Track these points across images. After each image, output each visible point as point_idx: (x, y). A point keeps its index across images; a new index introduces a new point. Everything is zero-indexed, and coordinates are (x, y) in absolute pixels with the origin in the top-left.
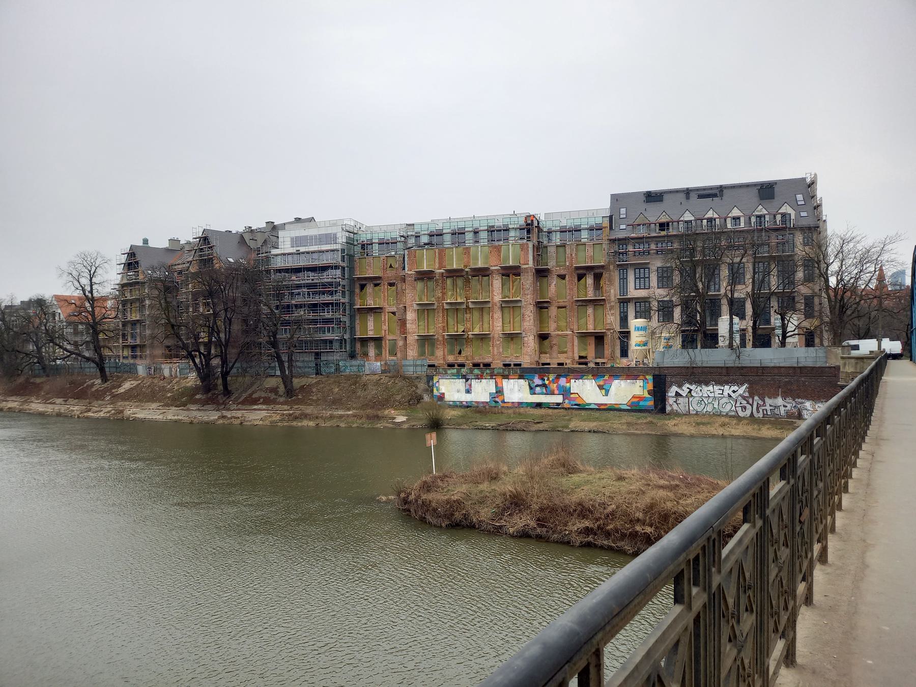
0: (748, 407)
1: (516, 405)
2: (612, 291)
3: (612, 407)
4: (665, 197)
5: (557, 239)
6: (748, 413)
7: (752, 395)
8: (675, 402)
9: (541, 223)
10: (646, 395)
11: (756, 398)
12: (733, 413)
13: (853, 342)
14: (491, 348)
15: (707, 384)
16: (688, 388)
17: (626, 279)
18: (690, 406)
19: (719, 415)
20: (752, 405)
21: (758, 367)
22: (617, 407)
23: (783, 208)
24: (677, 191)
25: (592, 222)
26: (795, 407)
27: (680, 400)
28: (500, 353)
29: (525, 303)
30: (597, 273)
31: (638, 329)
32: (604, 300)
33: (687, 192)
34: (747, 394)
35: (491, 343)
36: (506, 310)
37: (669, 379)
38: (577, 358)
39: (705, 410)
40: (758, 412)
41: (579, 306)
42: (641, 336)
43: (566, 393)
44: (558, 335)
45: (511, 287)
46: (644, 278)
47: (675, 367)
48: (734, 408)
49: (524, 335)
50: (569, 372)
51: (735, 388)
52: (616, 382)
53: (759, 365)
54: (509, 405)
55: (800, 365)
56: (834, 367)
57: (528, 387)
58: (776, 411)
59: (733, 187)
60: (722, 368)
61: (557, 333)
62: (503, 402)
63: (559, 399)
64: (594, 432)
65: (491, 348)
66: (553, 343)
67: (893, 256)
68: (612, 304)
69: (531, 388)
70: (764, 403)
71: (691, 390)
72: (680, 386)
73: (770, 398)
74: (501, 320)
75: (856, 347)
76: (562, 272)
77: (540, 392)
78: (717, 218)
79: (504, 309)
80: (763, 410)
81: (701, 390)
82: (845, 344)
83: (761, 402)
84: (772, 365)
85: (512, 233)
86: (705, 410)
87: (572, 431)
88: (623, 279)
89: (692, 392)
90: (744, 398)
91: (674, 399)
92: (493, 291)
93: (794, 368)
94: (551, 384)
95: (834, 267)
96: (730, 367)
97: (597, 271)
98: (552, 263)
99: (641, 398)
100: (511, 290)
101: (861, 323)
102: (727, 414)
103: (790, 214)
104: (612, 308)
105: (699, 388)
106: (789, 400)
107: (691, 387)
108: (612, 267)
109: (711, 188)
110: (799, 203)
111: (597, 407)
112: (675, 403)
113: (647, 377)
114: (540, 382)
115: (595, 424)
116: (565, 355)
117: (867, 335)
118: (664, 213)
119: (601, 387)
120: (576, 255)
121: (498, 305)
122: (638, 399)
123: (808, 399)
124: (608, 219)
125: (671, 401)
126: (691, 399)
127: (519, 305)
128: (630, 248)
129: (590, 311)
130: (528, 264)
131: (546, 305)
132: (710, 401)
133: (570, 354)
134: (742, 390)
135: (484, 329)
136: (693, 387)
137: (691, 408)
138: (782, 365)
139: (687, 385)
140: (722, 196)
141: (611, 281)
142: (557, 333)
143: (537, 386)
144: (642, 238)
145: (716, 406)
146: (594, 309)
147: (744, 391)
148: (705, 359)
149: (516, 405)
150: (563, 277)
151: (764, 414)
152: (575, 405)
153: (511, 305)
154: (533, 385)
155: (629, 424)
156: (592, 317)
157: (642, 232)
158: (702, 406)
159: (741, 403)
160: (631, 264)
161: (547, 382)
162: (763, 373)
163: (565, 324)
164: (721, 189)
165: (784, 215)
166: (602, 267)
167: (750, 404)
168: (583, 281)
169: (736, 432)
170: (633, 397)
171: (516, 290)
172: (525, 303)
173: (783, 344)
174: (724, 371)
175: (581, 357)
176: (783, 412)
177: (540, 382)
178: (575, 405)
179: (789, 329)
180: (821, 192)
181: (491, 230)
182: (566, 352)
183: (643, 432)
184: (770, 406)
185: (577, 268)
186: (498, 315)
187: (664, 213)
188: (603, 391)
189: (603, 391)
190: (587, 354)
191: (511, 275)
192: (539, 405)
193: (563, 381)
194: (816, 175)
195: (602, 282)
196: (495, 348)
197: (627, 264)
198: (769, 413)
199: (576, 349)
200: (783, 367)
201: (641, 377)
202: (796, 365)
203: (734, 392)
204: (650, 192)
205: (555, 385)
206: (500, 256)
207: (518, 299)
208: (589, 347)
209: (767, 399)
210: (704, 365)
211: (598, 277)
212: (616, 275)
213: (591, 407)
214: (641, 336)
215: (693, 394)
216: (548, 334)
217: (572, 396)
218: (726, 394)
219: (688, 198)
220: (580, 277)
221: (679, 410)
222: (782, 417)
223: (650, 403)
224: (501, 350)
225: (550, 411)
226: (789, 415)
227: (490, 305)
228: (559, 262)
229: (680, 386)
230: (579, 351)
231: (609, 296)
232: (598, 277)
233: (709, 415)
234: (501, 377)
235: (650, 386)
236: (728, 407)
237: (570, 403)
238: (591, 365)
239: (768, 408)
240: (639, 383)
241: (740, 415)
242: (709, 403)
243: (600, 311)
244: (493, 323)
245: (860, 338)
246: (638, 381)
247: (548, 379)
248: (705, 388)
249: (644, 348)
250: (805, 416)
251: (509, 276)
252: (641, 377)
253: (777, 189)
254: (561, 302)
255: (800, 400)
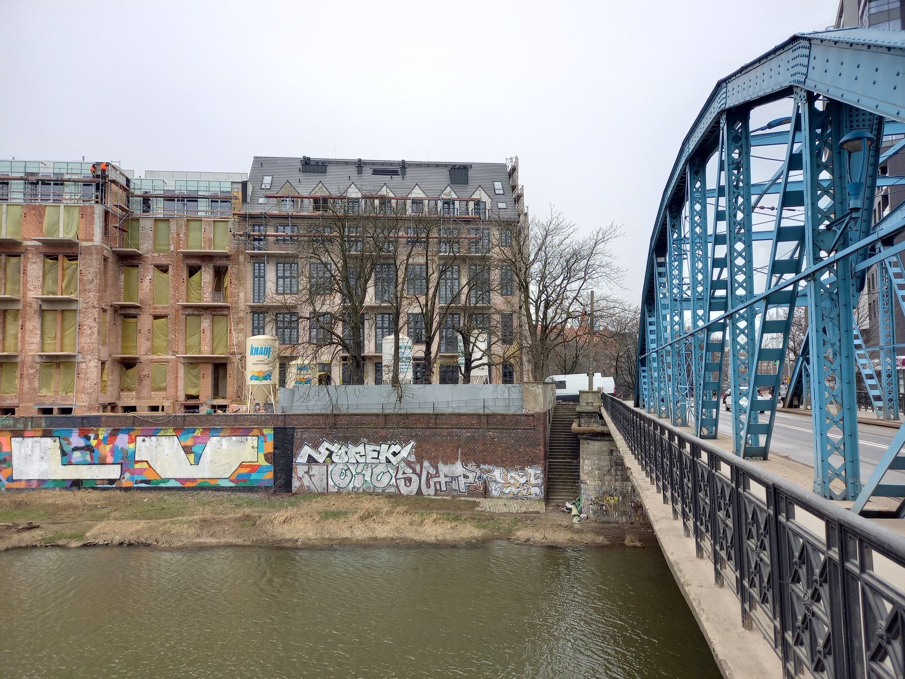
0: (415, 478)
1: (34, 485)
2: (242, 295)
3: (207, 485)
4: (330, 169)
5: (159, 209)
6: (414, 488)
7: (420, 460)
8: (307, 473)
9: (132, 185)
10: (263, 462)
11: (426, 464)
12: (393, 490)
13: (559, 378)
14: (17, 381)
15: (356, 443)
16: (327, 449)
17: (264, 277)
18: (329, 477)
19: (370, 494)
20: (420, 476)
21: (429, 415)
22: (212, 483)
23: (478, 192)
24: (346, 163)
25: (215, 189)
26: (480, 477)
27: (315, 469)
28: (34, 389)
29: (85, 305)
30: (219, 267)
31: (255, 351)
32: (228, 308)
33: (360, 165)
34: (413, 458)
35: (18, 374)
36: (49, 317)
37: (298, 435)
38: (182, 398)
39: (351, 486)
40: (428, 486)
41: (189, 315)
42: (261, 362)
43: (126, 461)
44: (153, 361)
45: (60, 277)
46: (291, 277)
47: (310, 415)
48: (393, 480)
49: (79, 358)
50: (134, 424)
51: (396, 448)
52: (214, 440)
53: (431, 411)
54: (22, 485)
55: (487, 412)
56: (533, 415)
57: (59, 452)
58: (454, 486)
59: (419, 165)
60: (377, 415)
61: (150, 357)
62: (10, 479)
63: (113, 472)
64: (130, 545)
65: (17, 381)
66: (144, 373)
67: (608, 259)
68: (241, 314)
69: (64, 453)
70: (437, 472)
71: (331, 453)
72: (316, 447)
73: (445, 463)
74: (39, 332)
75: (562, 385)
76: (163, 261)
77: (81, 460)
78: (393, 198)
79: (46, 314)
80: (435, 483)
81: (346, 453)
82: (548, 380)
83: (432, 471)
84: (450, 411)
85: (69, 189)
86: (351, 486)
87: (85, 546)
88: (259, 277)
89: (334, 456)
90: (409, 464)
91: (306, 468)
92: (25, 283)
93: (480, 415)
94: (102, 446)
95: (536, 268)
96: (389, 414)
97: (220, 263)
98: (146, 245)
99: (254, 468)
100: (60, 282)
101: (570, 353)
102: (383, 491)
103: (485, 202)
104: (240, 321)
105: (344, 449)
106: (472, 466)
107: (333, 448)
108: (241, 258)
109: (391, 164)
110: (497, 192)
111: (178, 484)
112: (306, 475)
113: (265, 432)
114: (81, 443)
115: (142, 524)
116: (162, 394)
117: (572, 368)
118: (320, 184)
119: (187, 450)
120: (186, 235)
121: (35, 306)
122: (249, 469)
123: (497, 465)
124: (240, 186)
125: (300, 471)
126: (330, 468)
127: (73, 307)
128: (271, 231)
129: (206, 323)
130: (92, 240)
131: (133, 312)
132: (359, 470)
133: (171, 391)
134: (406, 451)
135: (7, 348)
136: (334, 448)
137: (331, 483)
138: (463, 411)
139: (326, 445)
140: (404, 174)
141: (240, 279)
142: (150, 357)
143: (76, 449)
144: (286, 217)
145: (368, 478)
146: (213, 322)
147: (409, 454)
148: (353, 401)
149: (34, 485)
150: (164, 269)
151: (436, 490)
152: (142, 481)
153: (60, 307)
154: (67, 449)
155: (205, 523)
156: (208, 333)
157: (287, 208)
158: (348, 479)
159: (404, 473)
160: (270, 256)
161: (93, 443)
162: (436, 424)
163: (165, 344)
164: (404, 165)
165: (478, 203)
166: (227, 257)
167: (417, 474)
168: (196, 277)
169: (383, 531)
170: (241, 466)
171: (69, 282)
172: (85, 305)
173: (467, 379)
174: (381, 420)
175: (189, 397)
176: (463, 488)
177: (81, 443)
178: (142, 481)
179: (475, 356)
180: (523, 179)
181: (34, 182)
182: (165, 389)
183: (223, 540)
184: (446, 476)
185: (187, 256)
186: (33, 324)
187: (320, 184)
188: (192, 457)
189: (192, 457)
190: (199, 392)
191: (60, 257)
192: (77, 484)
193: (122, 440)
194: (517, 158)
195: (227, 281)
196: (26, 382)
197: (263, 255)
198: (444, 489)
199: (181, 383)
200: (464, 415)
201: (256, 432)
202: (481, 412)
203: (395, 454)
204: (309, 159)
205: (108, 447)
206: (41, 223)
207: (73, 297)
208: (202, 381)
209: (441, 466)
210: (351, 411)
211: (220, 274)
212: (248, 270)
213: (169, 484)
214: (261, 362)
215: (335, 458)
216: (136, 359)
217: (137, 466)
218: (382, 458)
219: (360, 172)
220: (193, 271)
221: (312, 487)
222: (461, 494)
223: (268, 476)
224: (36, 384)
225: (95, 495)
226: (471, 491)
227: (20, 306)
228: (159, 245)
229: (316, 447)
230: (186, 385)
231: (237, 302)
232: (220, 274)
233: (357, 493)
234: (9, 435)
235: (269, 447)
236: (386, 480)
237: (132, 479)
238: (204, 410)
239: (443, 480)
240: (252, 441)
241: (402, 492)
242: (358, 474)
243: (221, 324)
244: (23, 337)
245: (566, 373)
246: (249, 438)
247: (97, 437)
248: (353, 449)
249: (264, 382)
250: (493, 492)
251: (56, 259)
252: (256, 432)
253: (471, 173)
254: (158, 308)
255: (486, 467)
